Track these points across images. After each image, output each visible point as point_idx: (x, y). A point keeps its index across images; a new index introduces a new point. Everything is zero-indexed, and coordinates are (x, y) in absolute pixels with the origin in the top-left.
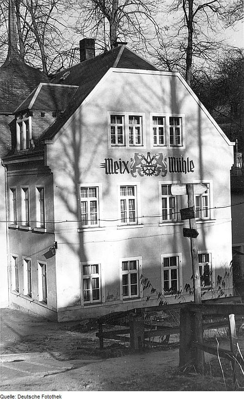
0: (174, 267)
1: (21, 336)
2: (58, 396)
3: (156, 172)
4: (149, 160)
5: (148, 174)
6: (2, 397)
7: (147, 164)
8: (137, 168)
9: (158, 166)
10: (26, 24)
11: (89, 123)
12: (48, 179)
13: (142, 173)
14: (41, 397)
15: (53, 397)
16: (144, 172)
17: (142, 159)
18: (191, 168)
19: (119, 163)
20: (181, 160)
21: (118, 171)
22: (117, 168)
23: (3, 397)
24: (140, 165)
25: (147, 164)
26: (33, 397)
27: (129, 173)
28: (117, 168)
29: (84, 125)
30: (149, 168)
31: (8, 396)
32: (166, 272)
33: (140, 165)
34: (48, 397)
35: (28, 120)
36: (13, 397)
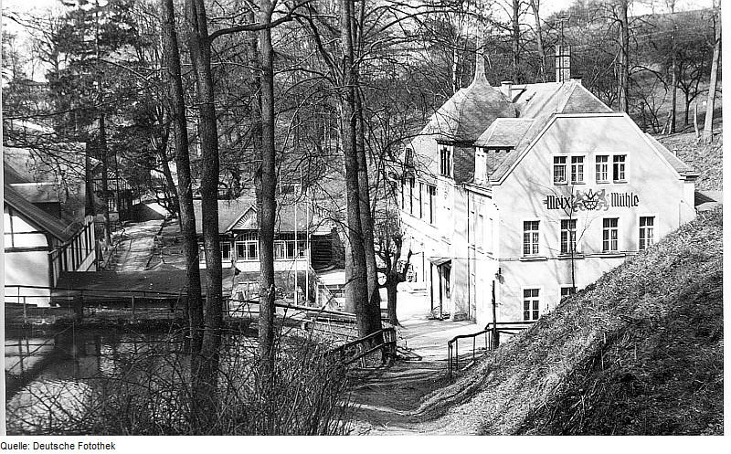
0: (535, 299)
1: (11, 215)
2: (108, 445)
3: (598, 207)
6: (4, 446)
9: (600, 201)
10: (275, 17)
13: (583, 208)
15: (99, 446)
21: (560, 206)
23: (7, 447)
26: (62, 447)
31: (15, 445)
32: (526, 303)
33: (581, 202)
34: (89, 446)
35: (615, 195)
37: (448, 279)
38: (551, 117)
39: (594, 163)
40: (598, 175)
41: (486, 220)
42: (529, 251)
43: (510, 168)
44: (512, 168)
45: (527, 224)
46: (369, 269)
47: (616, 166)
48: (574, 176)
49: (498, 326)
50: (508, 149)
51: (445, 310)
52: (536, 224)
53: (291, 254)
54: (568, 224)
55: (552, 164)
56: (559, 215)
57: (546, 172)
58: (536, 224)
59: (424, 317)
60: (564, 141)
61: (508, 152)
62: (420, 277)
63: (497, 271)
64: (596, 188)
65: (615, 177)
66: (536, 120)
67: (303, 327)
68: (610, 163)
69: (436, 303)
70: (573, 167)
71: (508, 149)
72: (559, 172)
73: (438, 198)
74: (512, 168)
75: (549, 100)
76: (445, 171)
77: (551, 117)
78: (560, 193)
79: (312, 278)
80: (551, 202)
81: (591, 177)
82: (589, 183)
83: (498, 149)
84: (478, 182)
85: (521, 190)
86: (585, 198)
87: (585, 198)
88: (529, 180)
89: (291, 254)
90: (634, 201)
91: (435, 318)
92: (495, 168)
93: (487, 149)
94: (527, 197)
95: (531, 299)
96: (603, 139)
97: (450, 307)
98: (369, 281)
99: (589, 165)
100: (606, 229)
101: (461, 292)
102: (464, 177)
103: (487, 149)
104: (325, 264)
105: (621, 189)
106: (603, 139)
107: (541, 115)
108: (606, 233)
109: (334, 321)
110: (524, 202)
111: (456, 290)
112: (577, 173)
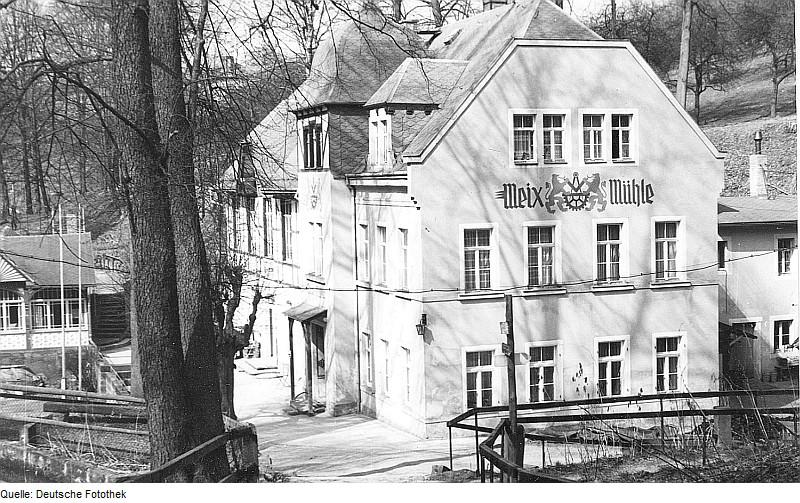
0: (486, 368)
2: (118, 494)
3: (588, 205)
4: (576, 186)
5: (573, 208)
6: (4, 494)
7: (573, 192)
8: (556, 198)
9: (592, 194)
11: (646, 329)
12: (359, 44)
13: (564, 205)
14: (84, 494)
15: (109, 494)
16: (569, 204)
17: (564, 184)
18: (647, 197)
19: (526, 191)
20: (631, 183)
22: (523, 198)
23: (7, 496)
24: (560, 195)
25: (573, 192)
26: (68, 495)
27: (542, 206)
28: (523, 198)
29: (625, 319)
30: (576, 198)
31: (17, 494)
32: (471, 377)
33: (560, 195)
34: (97, 494)
36: (26, 495)
37: (321, 346)
38: (508, 44)
39: (581, 129)
40: (587, 149)
41: (393, 234)
42: (473, 287)
43: (439, 134)
44: (444, 131)
45: (470, 235)
46: (181, 251)
47: (615, 134)
48: (547, 150)
49: (522, 413)
50: (428, 108)
51: (317, 397)
52: (484, 235)
53: (57, 321)
54: (541, 234)
55: (511, 128)
56: (526, 218)
57: (503, 141)
58: (484, 235)
59: (279, 412)
60: (535, 93)
61: (428, 113)
62: (265, 350)
63: (418, 320)
64: (587, 172)
65: (615, 154)
66: (472, 63)
67: (24, 436)
68: (606, 128)
69: (300, 388)
70: (547, 134)
71: (428, 108)
72: (523, 142)
73: (299, 218)
74: (444, 131)
75: (490, 33)
76: (313, 163)
77: (508, 44)
78: (526, 179)
79: (88, 356)
80: (510, 195)
81: (575, 155)
82: (573, 163)
83: (410, 108)
84: (377, 168)
85: (463, 179)
86: (567, 189)
87: (567, 189)
88: (476, 157)
89: (57, 321)
90: (645, 193)
91: (300, 413)
92: (406, 142)
93: (390, 108)
94: (472, 191)
95: (479, 369)
96: (599, 91)
97: (326, 393)
98: (180, 286)
99: (572, 135)
100: (602, 243)
101: (345, 365)
102: (349, 166)
103: (390, 108)
104: (113, 337)
105: (628, 175)
106: (599, 91)
107: (482, 52)
108: (601, 250)
109: (99, 420)
110: (468, 201)
111: (334, 363)
112: (553, 145)
